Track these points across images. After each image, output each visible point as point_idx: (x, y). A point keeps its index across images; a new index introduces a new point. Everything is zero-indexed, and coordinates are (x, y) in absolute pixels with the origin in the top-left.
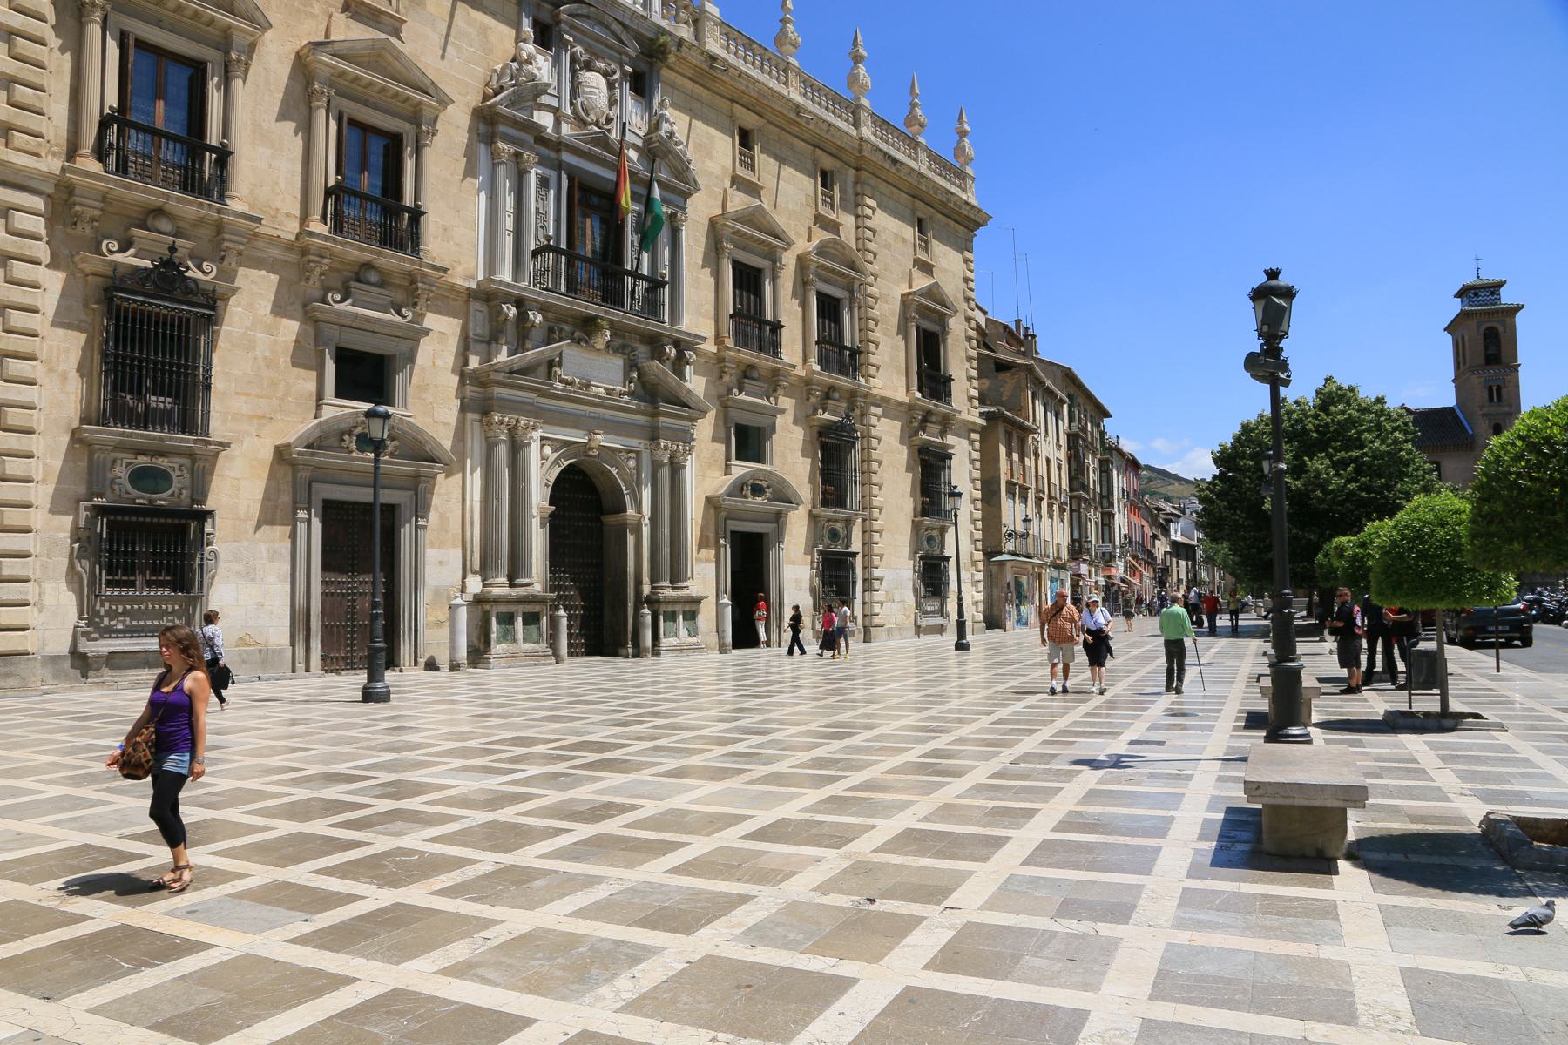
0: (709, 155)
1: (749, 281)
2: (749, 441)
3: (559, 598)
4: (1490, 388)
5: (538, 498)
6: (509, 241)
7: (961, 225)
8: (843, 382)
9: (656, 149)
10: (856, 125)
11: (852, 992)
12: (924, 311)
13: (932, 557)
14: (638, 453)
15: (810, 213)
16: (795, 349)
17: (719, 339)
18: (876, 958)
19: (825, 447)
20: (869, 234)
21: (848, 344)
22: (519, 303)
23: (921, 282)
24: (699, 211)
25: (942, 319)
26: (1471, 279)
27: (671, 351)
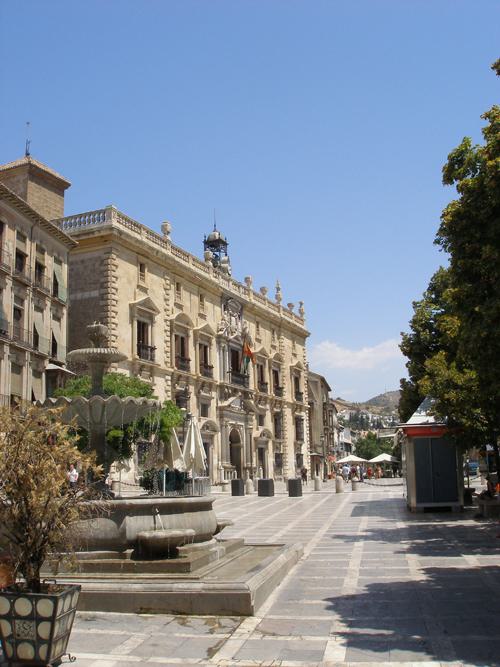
1: (142, 330)
7: (300, 336)
8: (279, 398)
15: (135, 284)
23: (141, 297)
25: (299, 372)
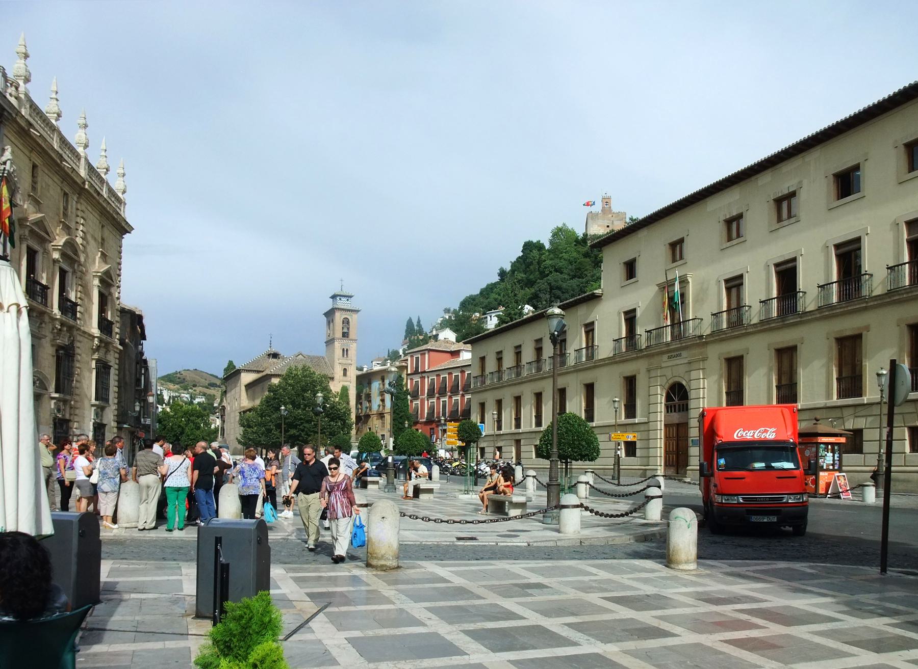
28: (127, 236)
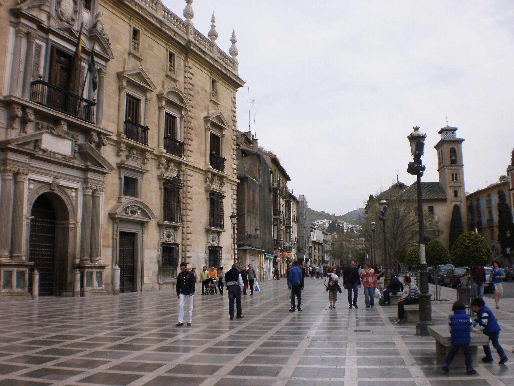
0: (118, 42)
2: (130, 186)
3: (35, 265)
4: (453, 175)
5: (26, 209)
6: (21, 76)
9: (94, 36)
10: (187, 33)
11: (229, 371)
12: (214, 125)
13: (213, 247)
14: (76, 189)
15: (163, 74)
16: (155, 141)
17: (119, 135)
18: (223, 379)
19: (165, 189)
20: (189, 86)
21: (178, 139)
22: (24, 108)
24: (113, 68)
26: (444, 126)
27: (96, 138)
28: (240, 89)
